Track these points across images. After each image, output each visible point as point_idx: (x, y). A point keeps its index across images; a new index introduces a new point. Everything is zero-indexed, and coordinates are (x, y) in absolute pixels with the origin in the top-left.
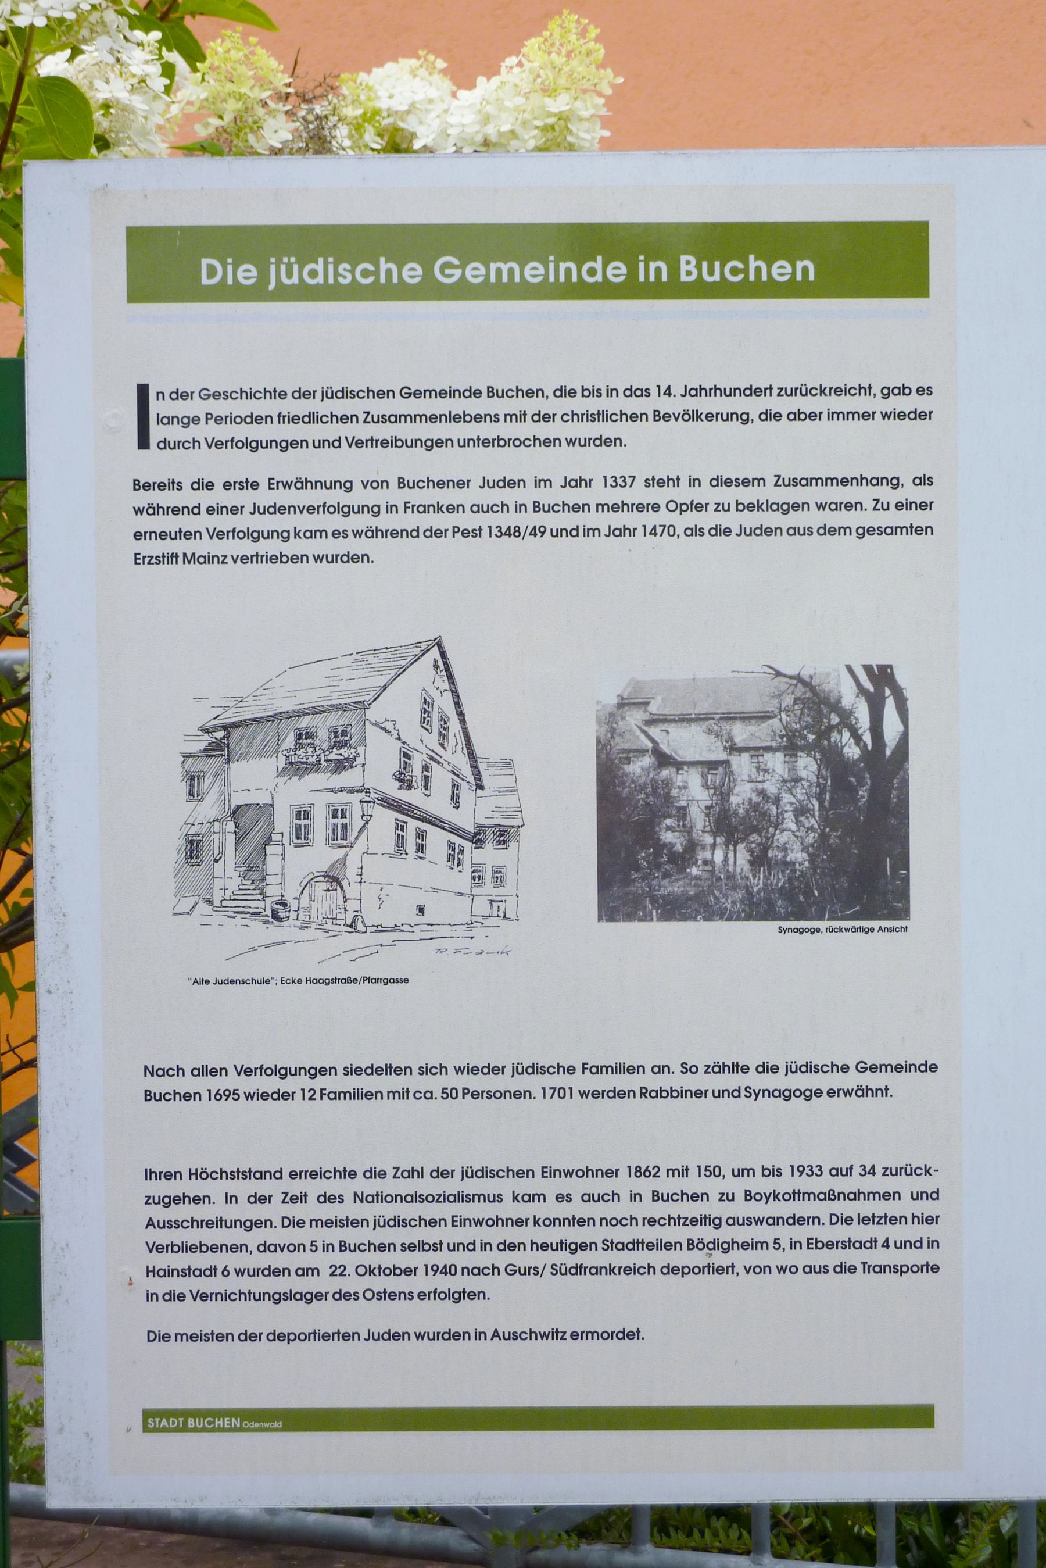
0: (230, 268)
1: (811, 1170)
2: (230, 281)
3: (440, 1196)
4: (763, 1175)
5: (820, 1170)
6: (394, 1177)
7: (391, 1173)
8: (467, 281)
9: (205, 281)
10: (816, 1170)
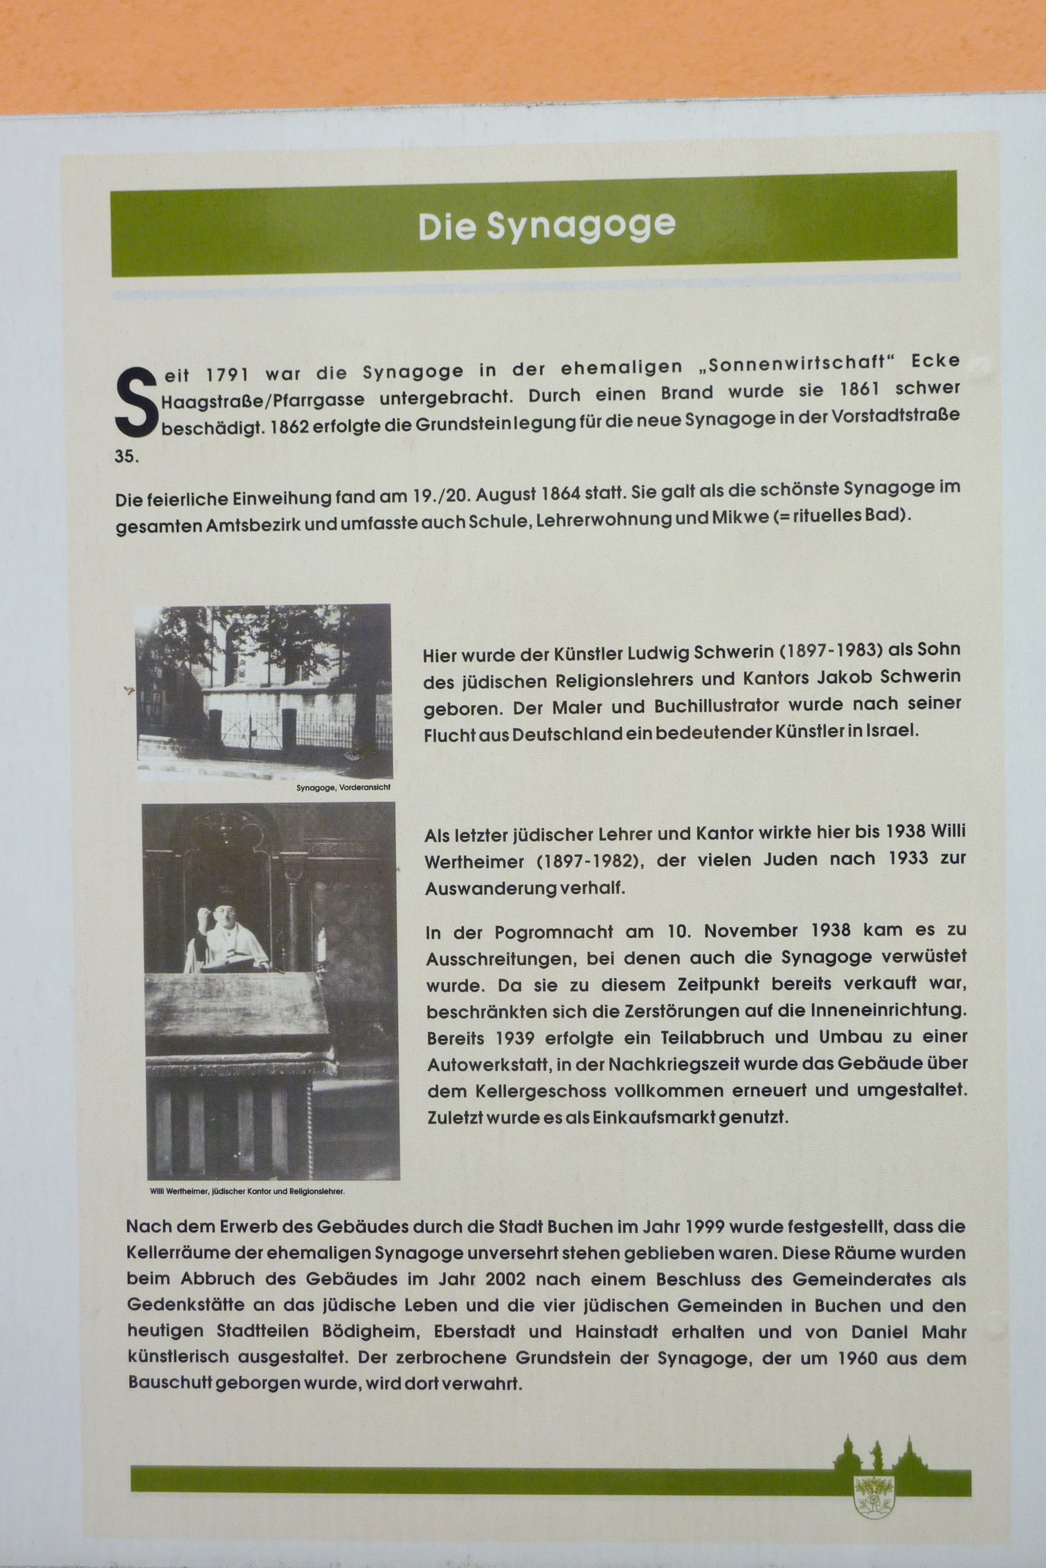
0: (448, 223)
1: (914, 857)
2: (449, 237)
3: (278, 523)
4: (858, 836)
5: (925, 857)
6: (628, 1016)
7: (624, 1011)
8: (659, 234)
9: (423, 236)
10: (920, 857)
